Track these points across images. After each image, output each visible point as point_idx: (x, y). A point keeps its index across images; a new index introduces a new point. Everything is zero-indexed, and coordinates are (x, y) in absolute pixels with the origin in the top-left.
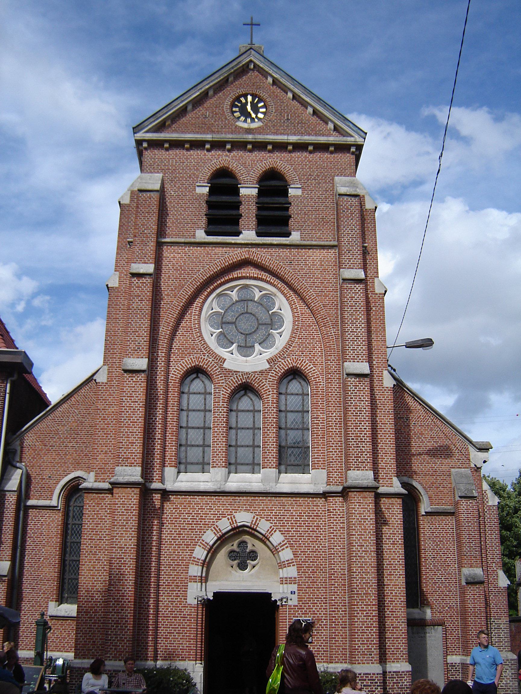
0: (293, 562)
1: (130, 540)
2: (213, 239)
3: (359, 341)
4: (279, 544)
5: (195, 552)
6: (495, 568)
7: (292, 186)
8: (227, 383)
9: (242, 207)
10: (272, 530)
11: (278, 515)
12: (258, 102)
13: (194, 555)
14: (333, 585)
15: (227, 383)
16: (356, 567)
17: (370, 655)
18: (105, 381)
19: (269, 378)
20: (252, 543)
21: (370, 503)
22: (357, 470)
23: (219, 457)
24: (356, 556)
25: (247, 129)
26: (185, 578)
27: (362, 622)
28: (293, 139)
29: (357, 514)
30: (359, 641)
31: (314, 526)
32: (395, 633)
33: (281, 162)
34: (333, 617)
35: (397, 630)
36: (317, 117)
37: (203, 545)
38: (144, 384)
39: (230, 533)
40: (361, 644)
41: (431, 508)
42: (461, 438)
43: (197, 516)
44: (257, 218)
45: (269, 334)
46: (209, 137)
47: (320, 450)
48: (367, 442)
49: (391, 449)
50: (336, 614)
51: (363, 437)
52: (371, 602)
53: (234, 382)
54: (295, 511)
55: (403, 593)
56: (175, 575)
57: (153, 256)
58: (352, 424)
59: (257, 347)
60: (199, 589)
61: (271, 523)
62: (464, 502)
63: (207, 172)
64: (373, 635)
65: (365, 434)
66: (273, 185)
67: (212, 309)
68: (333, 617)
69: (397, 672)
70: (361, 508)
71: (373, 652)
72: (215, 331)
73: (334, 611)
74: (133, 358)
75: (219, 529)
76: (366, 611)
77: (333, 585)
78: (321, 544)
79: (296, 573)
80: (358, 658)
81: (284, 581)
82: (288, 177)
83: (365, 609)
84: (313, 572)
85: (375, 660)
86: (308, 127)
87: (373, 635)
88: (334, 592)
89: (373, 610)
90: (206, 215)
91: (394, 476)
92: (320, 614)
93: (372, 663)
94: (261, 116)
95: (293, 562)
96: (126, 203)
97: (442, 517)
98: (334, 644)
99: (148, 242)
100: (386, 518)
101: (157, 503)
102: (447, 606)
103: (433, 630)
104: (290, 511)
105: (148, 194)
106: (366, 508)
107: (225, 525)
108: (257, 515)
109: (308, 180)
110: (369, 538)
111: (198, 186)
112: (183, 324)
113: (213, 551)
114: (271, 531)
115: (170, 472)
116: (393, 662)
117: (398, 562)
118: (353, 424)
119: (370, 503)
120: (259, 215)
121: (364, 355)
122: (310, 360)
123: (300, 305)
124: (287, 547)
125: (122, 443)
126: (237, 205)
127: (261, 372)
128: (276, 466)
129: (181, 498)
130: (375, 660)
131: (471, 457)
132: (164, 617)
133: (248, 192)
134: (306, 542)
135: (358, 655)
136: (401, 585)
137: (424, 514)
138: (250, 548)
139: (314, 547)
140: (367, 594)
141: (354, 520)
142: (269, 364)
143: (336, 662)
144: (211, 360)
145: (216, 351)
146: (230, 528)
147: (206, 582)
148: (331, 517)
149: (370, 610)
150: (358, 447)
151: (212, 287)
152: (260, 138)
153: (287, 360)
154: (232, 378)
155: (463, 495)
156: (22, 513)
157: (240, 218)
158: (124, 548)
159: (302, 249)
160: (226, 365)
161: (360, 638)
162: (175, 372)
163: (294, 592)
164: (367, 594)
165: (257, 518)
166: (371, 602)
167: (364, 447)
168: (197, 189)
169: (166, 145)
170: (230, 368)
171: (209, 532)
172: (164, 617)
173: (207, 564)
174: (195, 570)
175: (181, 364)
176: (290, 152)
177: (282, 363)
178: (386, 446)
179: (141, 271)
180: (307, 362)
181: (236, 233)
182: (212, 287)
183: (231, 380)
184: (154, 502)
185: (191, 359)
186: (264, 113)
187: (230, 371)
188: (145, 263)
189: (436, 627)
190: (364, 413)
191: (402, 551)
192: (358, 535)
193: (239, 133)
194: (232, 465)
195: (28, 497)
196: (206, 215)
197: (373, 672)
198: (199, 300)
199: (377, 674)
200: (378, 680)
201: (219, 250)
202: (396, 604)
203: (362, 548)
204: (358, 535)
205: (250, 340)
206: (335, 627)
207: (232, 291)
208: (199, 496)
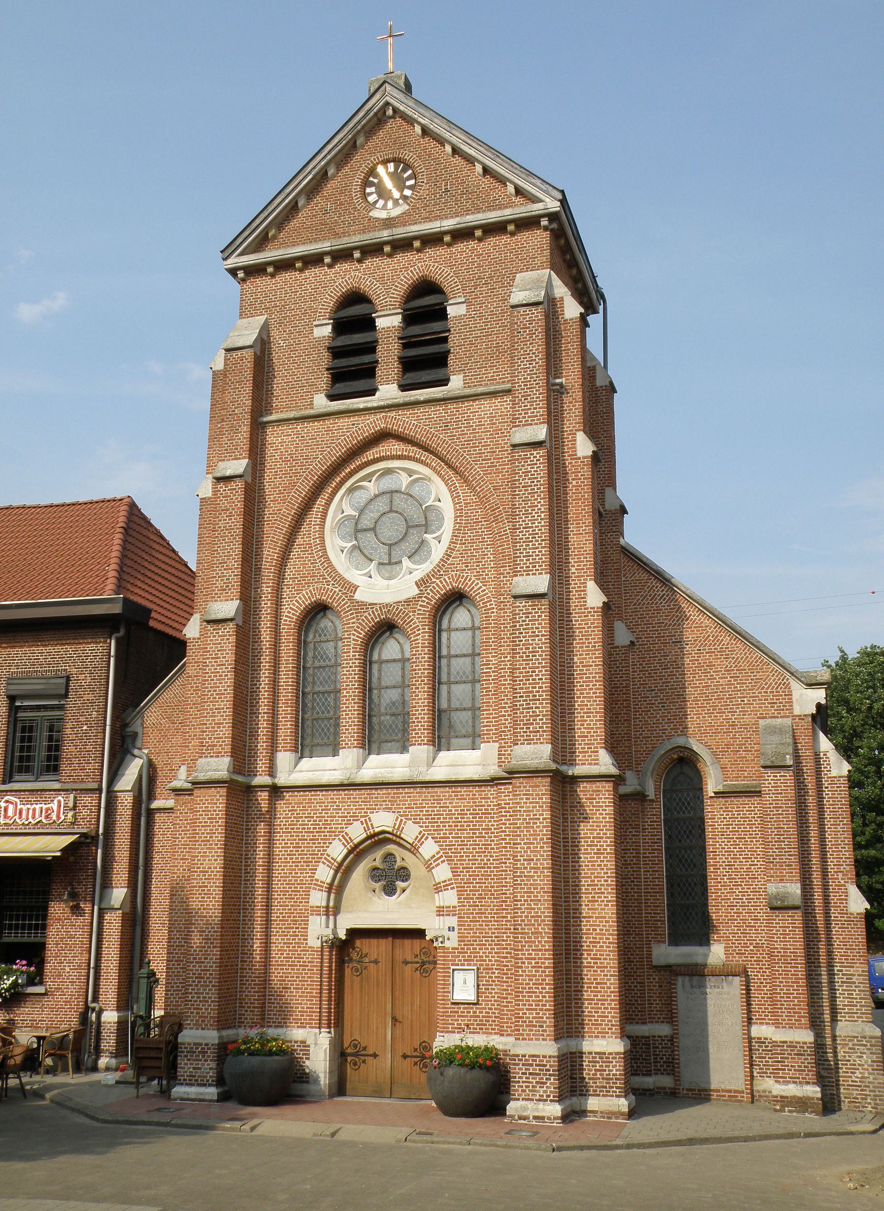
0: (452, 884)
1: (216, 860)
2: (343, 404)
3: (537, 541)
4: (432, 858)
5: (317, 872)
6: (842, 882)
7: (450, 302)
8: (360, 623)
9: (379, 348)
10: (422, 838)
11: (431, 815)
12: (404, 171)
13: (316, 877)
14: (503, 917)
15: (360, 623)
16: (520, 892)
17: (540, 1026)
18: (198, 636)
19: (419, 610)
20: (402, 857)
21: (542, 794)
22: (528, 744)
23: (349, 733)
24: (521, 876)
25: (386, 219)
26: (306, 910)
27: (528, 976)
28: (449, 224)
29: (524, 811)
30: (525, 1005)
31: (483, 829)
32: (600, 992)
33: (436, 264)
34: (505, 966)
35: (604, 988)
36: (491, 177)
37: (328, 861)
38: (233, 639)
39: (366, 843)
40: (527, 1009)
41: (724, 786)
42: (776, 667)
43: (320, 821)
44: (401, 363)
45: (423, 541)
46: (325, 246)
47: (492, 714)
48: (543, 700)
49: (597, 705)
50: (509, 962)
51: (538, 692)
52: (542, 946)
53: (370, 619)
54: (454, 807)
55: (613, 930)
56: (292, 906)
57: (247, 447)
58: (520, 673)
59: (406, 562)
60: (323, 925)
61: (421, 827)
62: (770, 775)
63: (328, 300)
64: (545, 997)
65: (540, 687)
66: (425, 305)
67: (343, 512)
68: (505, 966)
69: (601, 1054)
70: (531, 803)
71: (546, 1022)
72: (345, 545)
73: (506, 957)
74: (221, 601)
75: (350, 838)
76: (535, 959)
77: (503, 917)
78: (492, 856)
79: (457, 900)
80: (523, 1030)
81: (441, 912)
82: (446, 287)
83: (533, 956)
84: (480, 898)
85: (547, 1035)
86: (478, 197)
87: (545, 997)
88: (506, 929)
89: (545, 959)
90: (328, 369)
91: (602, 747)
92: (490, 961)
93: (543, 1039)
94: (407, 192)
95: (452, 884)
96: (219, 369)
97: (744, 798)
98: (505, 1006)
99: (240, 426)
100: (587, 814)
101: (264, 805)
102: (751, 944)
103: (724, 984)
104: (448, 807)
105: (239, 353)
106: (537, 803)
107: (357, 832)
108: (401, 816)
109: (476, 286)
110: (541, 847)
111: (316, 326)
112: (299, 540)
113: (344, 870)
114: (421, 838)
115: (284, 758)
116: (597, 1037)
117: (605, 881)
118: (522, 673)
119: (542, 794)
120: (403, 358)
121: (543, 562)
122: (478, 577)
123: (463, 491)
124: (443, 862)
125: (206, 724)
126: (371, 348)
127: (408, 601)
128: (428, 741)
129: (299, 796)
130: (547, 1035)
131: (795, 697)
132: (278, 965)
133: (388, 322)
134: (471, 853)
135: (522, 1026)
136: (610, 918)
137: (713, 795)
138: (399, 863)
139: (482, 860)
140: (536, 933)
141: (519, 822)
142: (419, 587)
143: (507, 1035)
144: (337, 590)
145: (346, 576)
146: (364, 835)
147: (335, 915)
148: (502, 816)
149: (541, 959)
150: (528, 708)
151: (338, 479)
152: (401, 232)
153: (445, 580)
154: (366, 614)
155: (769, 763)
156: (143, 819)
157: (376, 367)
158: (207, 872)
159: (463, 402)
160: (358, 596)
161: (527, 1001)
162: (289, 612)
163: (453, 928)
164: (536, 933)
165: (401, 820)
166: (542, 946)
167: (538, 708)
168: (316, 330)
169: (270, 270)
170: (363, 600)
171: (336, 843)
172: (278, 965)
173: (337, 889)
174: (318, 898)
175: (297, 601)
176: (449, 245)
177: (437, 585)
178: (589, 701)
179: (228, 473)
180: (473, 578)
181: (368, 391)
182: (338, 479)
183: (366, 617)
184: (259, 804)
185: (310, 591)
186: (411, 188)
187: (363, 604)
188: (236, 459)
189: (730, 978)
190: (540, 656)
191: (611, 865)
192: (525, 844)
193: (374, 229)
194: (370, 741)
195: (151, 797)
196: (328, 369)
197: (544, 1054)
198: (321, 501)
199: (550, 1057)
200: (550, 1066)
201: (344, 422)
202: (602, 947)
203: (530, 864)
204: (525, 844)
205: (396, 553)
206: (507, 982)
207: (370, 481)
208: (322, 791)
